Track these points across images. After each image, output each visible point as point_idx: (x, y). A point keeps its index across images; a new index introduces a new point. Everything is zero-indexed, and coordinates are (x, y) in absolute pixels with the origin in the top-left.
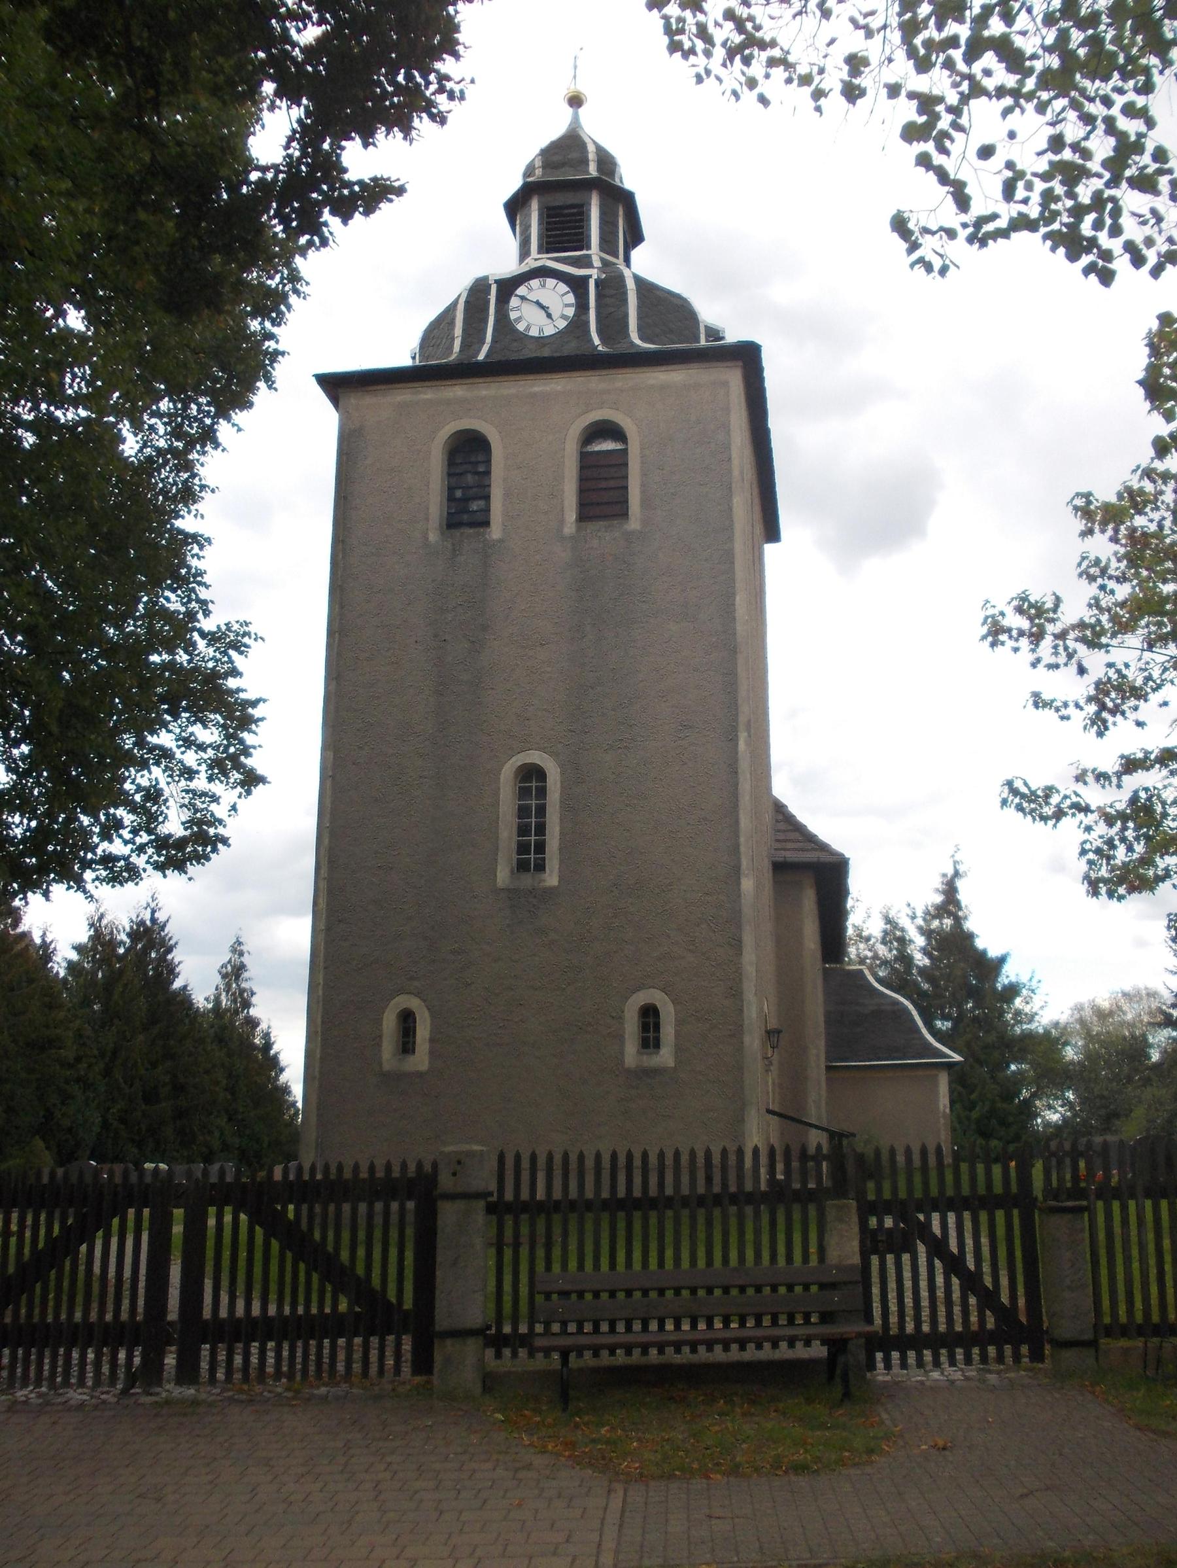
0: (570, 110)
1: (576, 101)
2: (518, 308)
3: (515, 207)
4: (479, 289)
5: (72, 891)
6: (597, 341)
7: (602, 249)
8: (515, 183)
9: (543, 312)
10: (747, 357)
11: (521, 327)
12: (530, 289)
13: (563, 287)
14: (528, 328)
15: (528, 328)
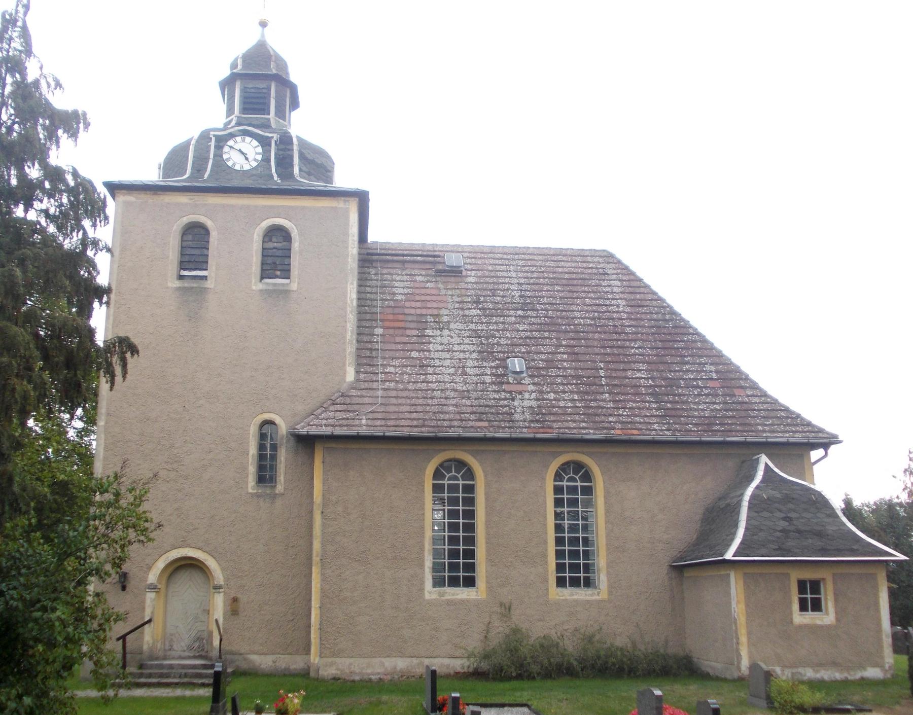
0: (260, 28)
1: (263, 24)
2: (228, 153)
3: (227, 85)
4: (205, 137)
5: (894, 496)
6: (276, 178)
7: (276, 115)
8: (226, 73)
9: (244, 155)
10: (362, 198)
11: (230, 164)
12: (236, 142)
13: (255, 143)
14: (234, 164)
15: (234, 164)
